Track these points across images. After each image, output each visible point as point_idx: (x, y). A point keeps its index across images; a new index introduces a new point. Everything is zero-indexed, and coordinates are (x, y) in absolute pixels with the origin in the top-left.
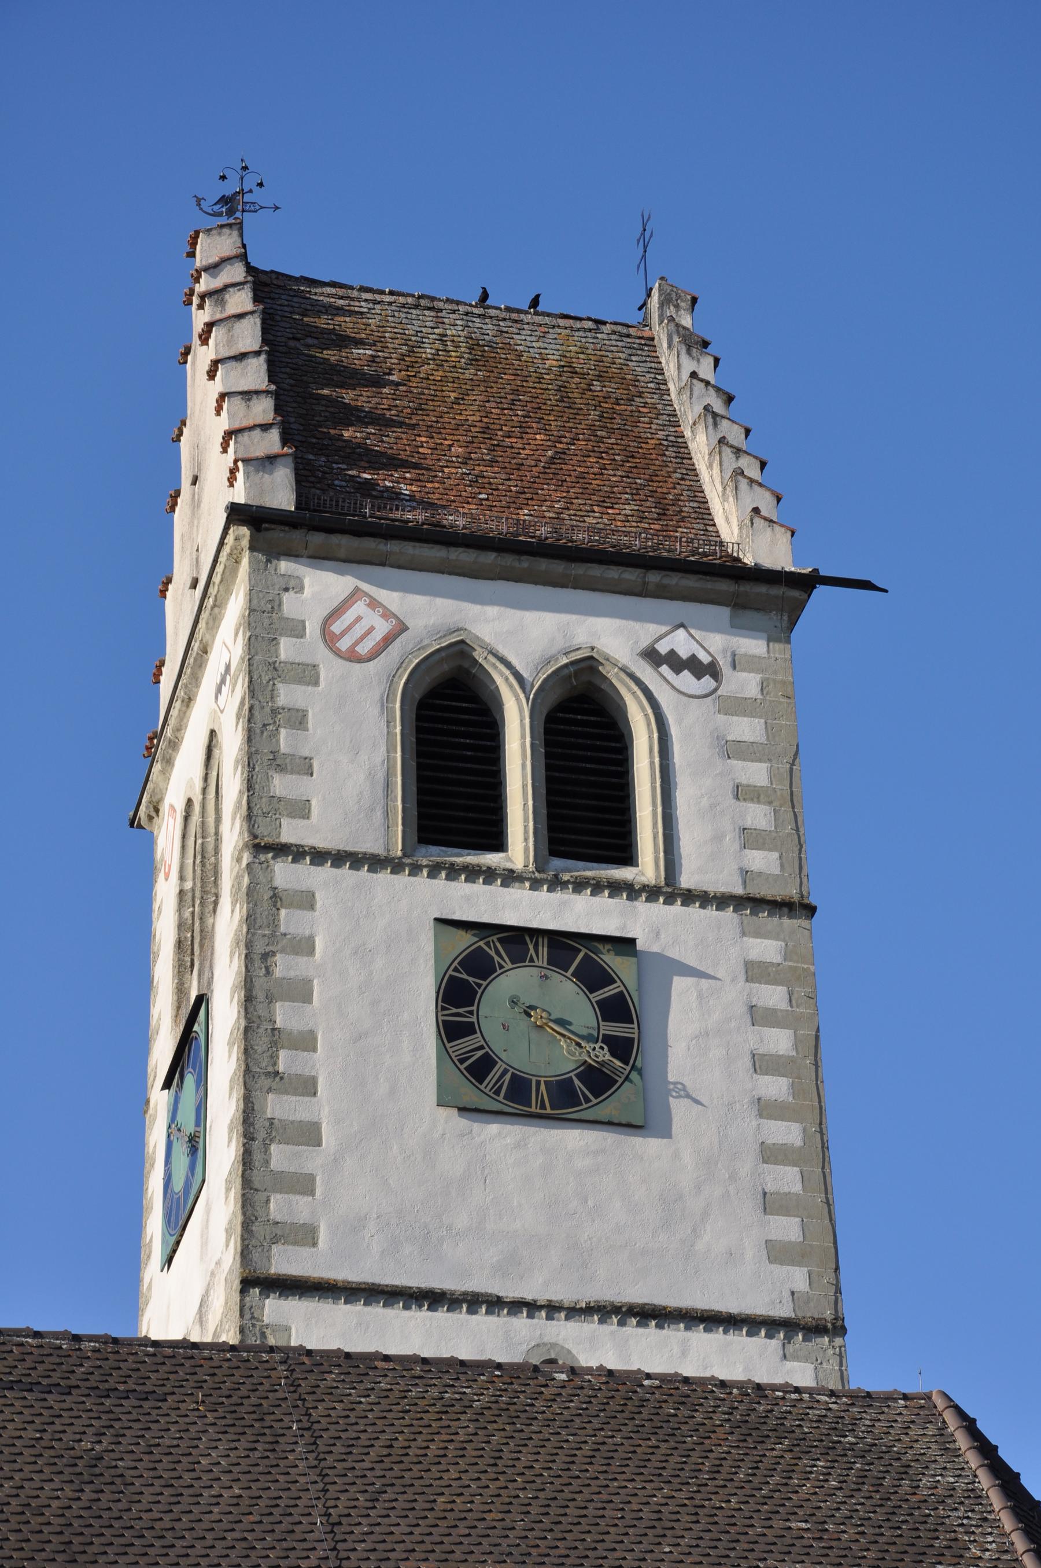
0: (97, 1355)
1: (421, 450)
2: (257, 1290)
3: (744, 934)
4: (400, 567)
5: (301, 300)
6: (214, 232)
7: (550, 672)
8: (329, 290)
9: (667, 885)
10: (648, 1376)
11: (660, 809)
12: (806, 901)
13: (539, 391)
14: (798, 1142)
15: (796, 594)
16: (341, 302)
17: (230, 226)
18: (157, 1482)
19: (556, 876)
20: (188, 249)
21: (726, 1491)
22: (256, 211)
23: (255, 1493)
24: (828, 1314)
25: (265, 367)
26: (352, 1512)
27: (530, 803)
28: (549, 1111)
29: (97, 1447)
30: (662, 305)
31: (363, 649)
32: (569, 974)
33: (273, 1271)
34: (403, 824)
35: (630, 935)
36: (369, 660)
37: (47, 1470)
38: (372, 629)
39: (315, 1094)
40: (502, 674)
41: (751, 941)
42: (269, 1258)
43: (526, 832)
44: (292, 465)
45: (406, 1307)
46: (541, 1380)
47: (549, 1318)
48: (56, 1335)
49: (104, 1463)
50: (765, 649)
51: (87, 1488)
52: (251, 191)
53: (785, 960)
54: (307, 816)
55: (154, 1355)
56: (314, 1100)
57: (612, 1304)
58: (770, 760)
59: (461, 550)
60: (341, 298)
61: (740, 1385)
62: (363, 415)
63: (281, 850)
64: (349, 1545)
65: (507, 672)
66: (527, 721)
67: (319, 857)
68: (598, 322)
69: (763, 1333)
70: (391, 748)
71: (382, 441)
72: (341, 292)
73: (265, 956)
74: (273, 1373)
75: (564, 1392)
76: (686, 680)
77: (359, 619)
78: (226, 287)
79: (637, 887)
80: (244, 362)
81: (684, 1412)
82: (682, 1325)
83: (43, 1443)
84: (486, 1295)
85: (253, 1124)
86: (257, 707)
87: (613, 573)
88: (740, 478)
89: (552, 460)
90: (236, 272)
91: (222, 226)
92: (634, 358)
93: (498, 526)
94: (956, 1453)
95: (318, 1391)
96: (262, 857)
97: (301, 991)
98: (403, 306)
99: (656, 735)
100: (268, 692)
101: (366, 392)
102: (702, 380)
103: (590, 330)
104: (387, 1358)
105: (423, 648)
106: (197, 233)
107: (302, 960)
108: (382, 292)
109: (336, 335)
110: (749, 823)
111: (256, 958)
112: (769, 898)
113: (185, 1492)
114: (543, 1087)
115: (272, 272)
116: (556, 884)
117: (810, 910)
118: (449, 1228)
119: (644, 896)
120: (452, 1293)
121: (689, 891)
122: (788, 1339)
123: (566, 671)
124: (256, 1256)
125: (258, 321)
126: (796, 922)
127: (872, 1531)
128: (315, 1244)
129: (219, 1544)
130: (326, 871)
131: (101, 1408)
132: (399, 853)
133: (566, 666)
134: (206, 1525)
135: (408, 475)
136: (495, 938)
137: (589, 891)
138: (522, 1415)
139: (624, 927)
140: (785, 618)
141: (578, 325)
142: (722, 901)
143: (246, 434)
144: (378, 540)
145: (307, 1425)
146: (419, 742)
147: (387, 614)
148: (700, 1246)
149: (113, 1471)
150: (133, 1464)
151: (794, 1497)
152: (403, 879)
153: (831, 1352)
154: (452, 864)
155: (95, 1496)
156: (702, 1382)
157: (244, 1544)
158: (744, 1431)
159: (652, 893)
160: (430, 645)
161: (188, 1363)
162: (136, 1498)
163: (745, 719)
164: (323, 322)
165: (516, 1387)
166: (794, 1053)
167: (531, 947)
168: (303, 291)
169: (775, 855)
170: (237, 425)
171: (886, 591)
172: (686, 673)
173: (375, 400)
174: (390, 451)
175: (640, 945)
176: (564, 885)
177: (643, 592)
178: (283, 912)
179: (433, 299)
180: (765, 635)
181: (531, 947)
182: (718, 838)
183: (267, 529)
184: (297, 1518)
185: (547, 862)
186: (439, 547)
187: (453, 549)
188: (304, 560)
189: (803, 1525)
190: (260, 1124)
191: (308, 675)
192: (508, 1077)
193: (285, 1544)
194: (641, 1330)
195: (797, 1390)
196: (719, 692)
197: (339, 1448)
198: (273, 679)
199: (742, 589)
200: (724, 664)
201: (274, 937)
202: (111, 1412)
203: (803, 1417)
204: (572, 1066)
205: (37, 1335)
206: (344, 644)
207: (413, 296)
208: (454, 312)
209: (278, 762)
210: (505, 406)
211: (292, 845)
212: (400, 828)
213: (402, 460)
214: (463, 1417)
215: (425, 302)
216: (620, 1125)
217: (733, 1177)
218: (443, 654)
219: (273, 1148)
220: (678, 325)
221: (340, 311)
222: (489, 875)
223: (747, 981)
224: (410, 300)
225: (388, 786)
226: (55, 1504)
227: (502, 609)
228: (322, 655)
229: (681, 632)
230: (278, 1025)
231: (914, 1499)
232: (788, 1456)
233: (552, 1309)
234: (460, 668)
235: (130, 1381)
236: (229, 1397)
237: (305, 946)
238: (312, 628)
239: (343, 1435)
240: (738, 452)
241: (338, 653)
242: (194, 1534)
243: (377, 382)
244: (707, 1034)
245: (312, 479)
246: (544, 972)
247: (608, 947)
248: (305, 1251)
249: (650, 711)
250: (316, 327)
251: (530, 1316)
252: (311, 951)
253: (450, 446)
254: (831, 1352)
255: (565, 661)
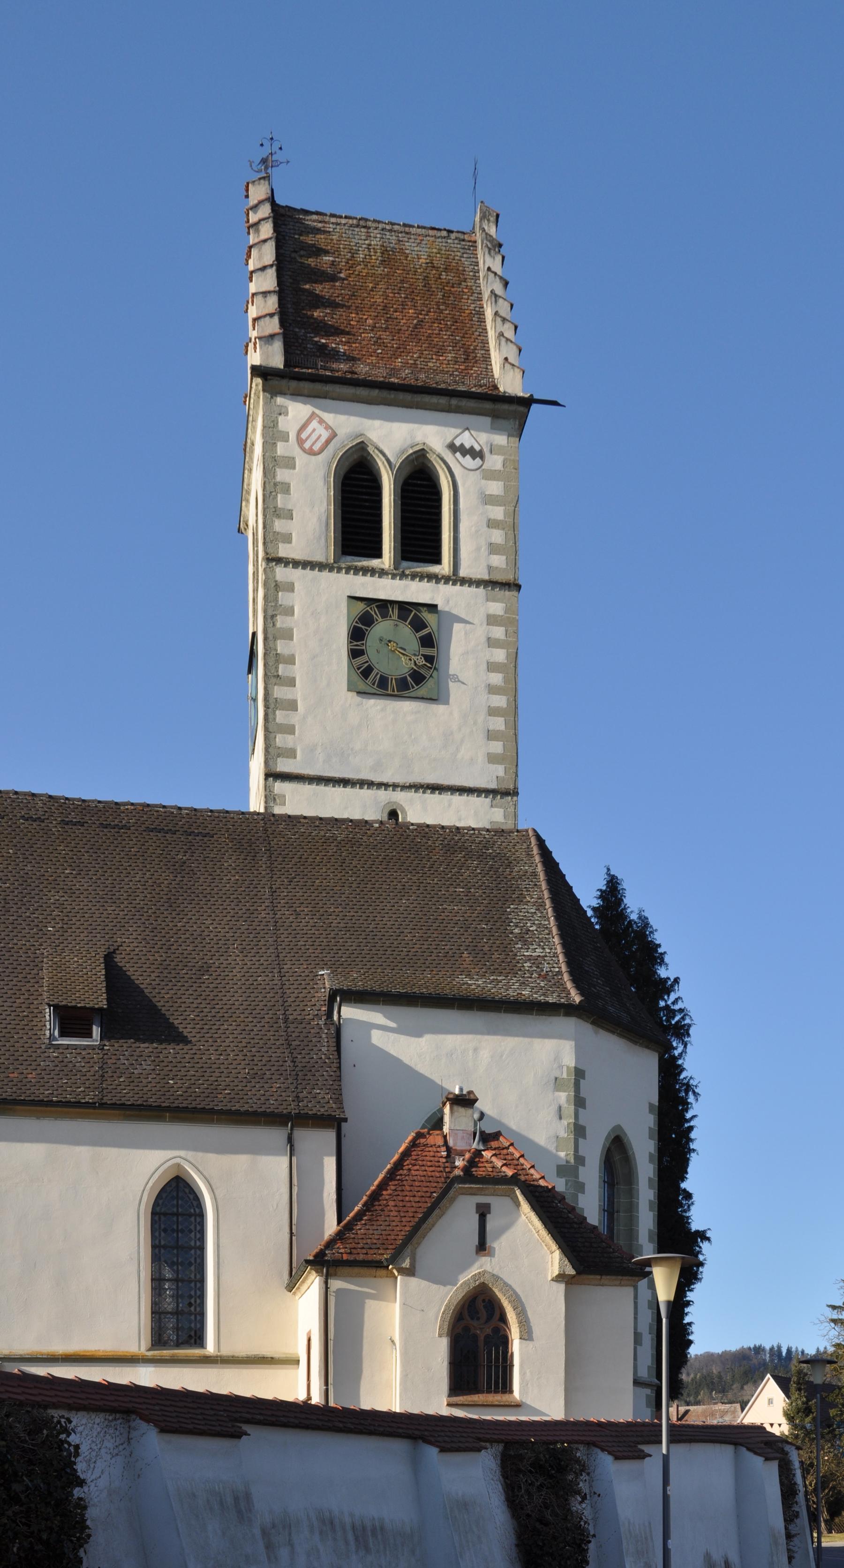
0: (188, 816)
1: (352, 323)
2: (271, 779)
3: (487, 600)
4: (333, 399)
5: (300, 225)
6: (256, 183)
7: (403, 458)
8: (315, 217)
9: (454, 575)
10: (412, 824)
11: (452, 534)
12: (517, 582)
13: (414, 280)
14: (505, 706)
15: (522, 409)
16: (320, 225)
17: (264, 178)
18: (206, 873)
19: (403, 572)
20: (245, 193)
21: (434, 876)
22: (278, 166)
23: (244, 878)
24: (512, 787)
25: (275, 274)
26: (281, 887)
27: (392, 532)
28: (396, 693)
29: (184, 858)
30: (481, 220)
31: (316, 448)
32: (407, 623)
33: (278, 770)
34: (334, 545)
35: (435, 603)
36: (319, 453)
37: (164, 867)
38: (320, 436)
39: (295, 686)
40: (381, 460)
41: (490, 604)
42: (276, 764)
43: (390, 548)
44: (282, 340)
45: (334, 786)
46: (368, 827)
47: (394, 790)
48: (172, 807)
49: (186, 865)
50: (506, 441)
51: (179, 876)
52: (275, 153)
53: (505, 613)
54: (290, 542)
55: (211, 816)
56: (295, 689)
57: (420, 784)
58: (505, 505)
59: (361, 388)
60: (320, 222)
61: (450, 828)
62: (325, 300)
63: (279, 560)
64: (278, 901)
65: (383, 459)
66: (392, 486)
67: (296, 564)
68: (450, 232)
69: (483, 795)
70: (328, 504)
71: (333, 318)
72: (320, 218)
73: (273, 617)
74: (258, 825)
75: (376, 832)
76: (468, 461)
77: (314, 430)
78: (260, 220)
79: (440, 577)
80: (265, 272)
81: (424, 840)
82: (449, 793)
83: (163, 856)
84: (367, 780)
85: (268, 701)
86: (267, 483)
87: (434, 399)
88: (502, 338)
89: (415, 327)
90: (265, 211)
91: (260, 179)
92: (465, 255)
93: (380, 374)
94: (532, 856)
95: (275, 833)
96: (271, 565)
97: (288, 635)
98: (351, 226)
99: (452, 493)
100: (272, 473)
101: (327, 285)
102: (493, 272)
103: (444, 237)
104: (305, 818)
105: (344, 446)
106: (248, 184)
107: (289, 618)
108: (341, 217)
109: (316, 247)
110: (493, 540)
111: (269, 617)
112: (500, 581)
113: (217, 877)
114: (394, 681)
115: (287, 206)
116: (403, 576)
117: (518, 587)
118: (352, 749)
119: (443, 581)
120: (353, 779)
121: (463, 578)
122: (494, 798)
123: (411, 458)
124: (271, 763)
125: (274, 244)
126: (511, 593)
127: (489, 891)
128: (295, 757)
129: (228, 900)
130: (299, 572)
131: (187, 840)
132: (332, 561)
133: (411, 454)
134: (223, 892)
135: (344, 340)
136: (374, 605)
137: (418, 579)
138: (357, 843)
139: (433, 598)
140: (517, 423)
141: (439, 234)
142: (478, 583)
143: (262, 320)
144: (322, 384)
145: (268, 848)
146: (343, 498)
147: (328, 427)
148: (459, 756)
149: (189, 868)
150: (197, 865)
151: (461, 877)
152: (334, 575)
153: (511, 803)
154: (356, 567)
155: (181, 879)
156: (434, 826)
157: (237, 900)
158: (447, 848)
159: (447, 580)
160: (348, 444)
161: (224, 820)
162: (197, 880)
163: (495, 482)
164: (310, 239)
165: (357, 830)
166: (506, 661)
167: (390, 610)
168: (301, 219)
169: (504, 557)
170: (260, 314)
171: (564, 406)
172: (468, 457)
173: (331, 291)
174: (336, 324)
175: (439, 608)
176: (407, 576)
177: (449, 410)
178: (280, 594)
179: (366, 220)
180: (507, 433)
181: (390, 610)
182: (478, 549)
183: (270, 379)
184: (259, 889)
185: (400, 564)
186: (351, 387)
187: (358, 388)
188: (288, 396)
189: (462, 890)
190: (271, 701)
191: (290, 463)
192: (379, 676)
193: (253, 900)
194: (432, 795)
195: (473, 829)
196: (483, 467)
197: (280, 859)
198: (274, 466)
199: (496, 407)
200: (486, 451)
201: (276, 607)
202: (191, 842)
203: (473, 842)
204: (407, 670)
205: (164, 807)
206: (307, 445)
207: (356, 218)
208: (376, 228)
209: (277, 513)
210: (396, 291)
211: (283, 558)
212: (333, 547)
213: (341, 330)
214: (332, 844)
215: (362, 223)
216: (427, 699)
217: (475, 723)
218: (354, 449)
219: (278, 712)
220: (487, 234)
221: (318, 231)
222: (372, 572)
223: (487, 624)
224: (355, 222)
225: (327, 524)
226: (166, 882)
227: (382, 422)
228: (297, 452)
229: (467, 432)
230: (278, 652)
231: (509, 877)
232: (463, 859)
233: (395, 786)
234: (362, 456)
235: (200, 828)
236: (239, 835)
237: (290, 611)
238: (292, 436)
239: (283, 853)
240: (504, 320)
241: (304, 450)
242: (219, 896)
243: (333, 278)
244: (468, 653)
245: (296, 344)
246: (396, 622)
247: (425, 609)
248: (291, 761)
249: (450, 479)
250: (306, 243)
251: (386, 790)
252: (293, 614)
253: (366, 319)
254: (511, 803)
255: (411, 451)
